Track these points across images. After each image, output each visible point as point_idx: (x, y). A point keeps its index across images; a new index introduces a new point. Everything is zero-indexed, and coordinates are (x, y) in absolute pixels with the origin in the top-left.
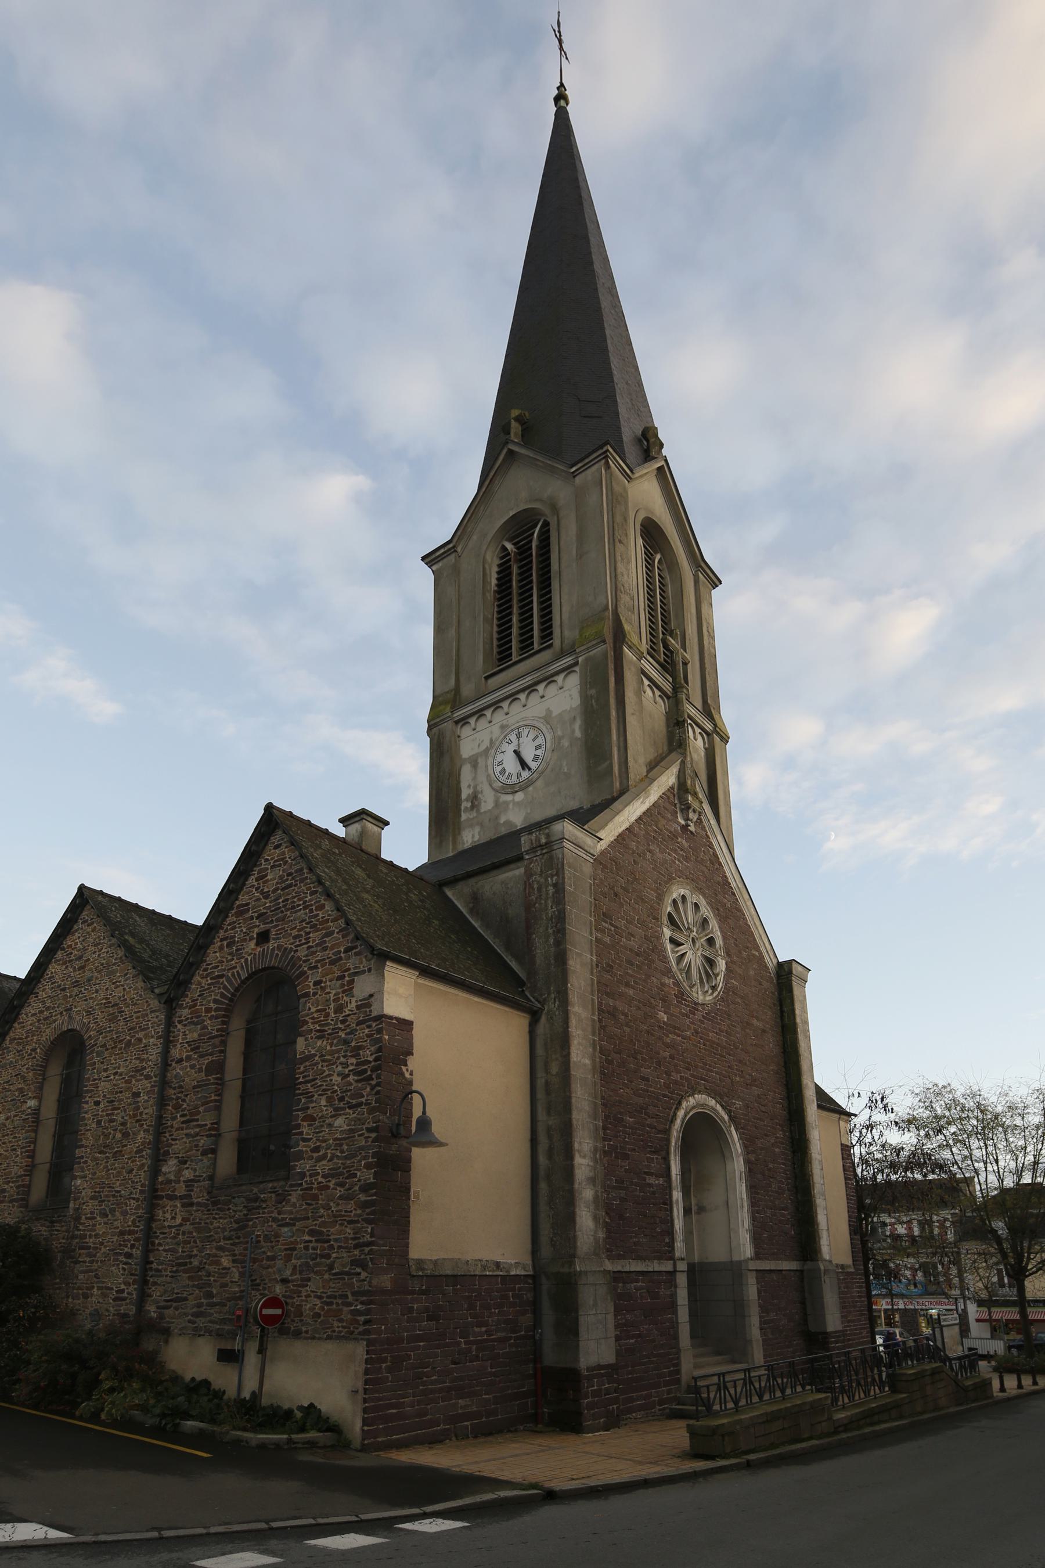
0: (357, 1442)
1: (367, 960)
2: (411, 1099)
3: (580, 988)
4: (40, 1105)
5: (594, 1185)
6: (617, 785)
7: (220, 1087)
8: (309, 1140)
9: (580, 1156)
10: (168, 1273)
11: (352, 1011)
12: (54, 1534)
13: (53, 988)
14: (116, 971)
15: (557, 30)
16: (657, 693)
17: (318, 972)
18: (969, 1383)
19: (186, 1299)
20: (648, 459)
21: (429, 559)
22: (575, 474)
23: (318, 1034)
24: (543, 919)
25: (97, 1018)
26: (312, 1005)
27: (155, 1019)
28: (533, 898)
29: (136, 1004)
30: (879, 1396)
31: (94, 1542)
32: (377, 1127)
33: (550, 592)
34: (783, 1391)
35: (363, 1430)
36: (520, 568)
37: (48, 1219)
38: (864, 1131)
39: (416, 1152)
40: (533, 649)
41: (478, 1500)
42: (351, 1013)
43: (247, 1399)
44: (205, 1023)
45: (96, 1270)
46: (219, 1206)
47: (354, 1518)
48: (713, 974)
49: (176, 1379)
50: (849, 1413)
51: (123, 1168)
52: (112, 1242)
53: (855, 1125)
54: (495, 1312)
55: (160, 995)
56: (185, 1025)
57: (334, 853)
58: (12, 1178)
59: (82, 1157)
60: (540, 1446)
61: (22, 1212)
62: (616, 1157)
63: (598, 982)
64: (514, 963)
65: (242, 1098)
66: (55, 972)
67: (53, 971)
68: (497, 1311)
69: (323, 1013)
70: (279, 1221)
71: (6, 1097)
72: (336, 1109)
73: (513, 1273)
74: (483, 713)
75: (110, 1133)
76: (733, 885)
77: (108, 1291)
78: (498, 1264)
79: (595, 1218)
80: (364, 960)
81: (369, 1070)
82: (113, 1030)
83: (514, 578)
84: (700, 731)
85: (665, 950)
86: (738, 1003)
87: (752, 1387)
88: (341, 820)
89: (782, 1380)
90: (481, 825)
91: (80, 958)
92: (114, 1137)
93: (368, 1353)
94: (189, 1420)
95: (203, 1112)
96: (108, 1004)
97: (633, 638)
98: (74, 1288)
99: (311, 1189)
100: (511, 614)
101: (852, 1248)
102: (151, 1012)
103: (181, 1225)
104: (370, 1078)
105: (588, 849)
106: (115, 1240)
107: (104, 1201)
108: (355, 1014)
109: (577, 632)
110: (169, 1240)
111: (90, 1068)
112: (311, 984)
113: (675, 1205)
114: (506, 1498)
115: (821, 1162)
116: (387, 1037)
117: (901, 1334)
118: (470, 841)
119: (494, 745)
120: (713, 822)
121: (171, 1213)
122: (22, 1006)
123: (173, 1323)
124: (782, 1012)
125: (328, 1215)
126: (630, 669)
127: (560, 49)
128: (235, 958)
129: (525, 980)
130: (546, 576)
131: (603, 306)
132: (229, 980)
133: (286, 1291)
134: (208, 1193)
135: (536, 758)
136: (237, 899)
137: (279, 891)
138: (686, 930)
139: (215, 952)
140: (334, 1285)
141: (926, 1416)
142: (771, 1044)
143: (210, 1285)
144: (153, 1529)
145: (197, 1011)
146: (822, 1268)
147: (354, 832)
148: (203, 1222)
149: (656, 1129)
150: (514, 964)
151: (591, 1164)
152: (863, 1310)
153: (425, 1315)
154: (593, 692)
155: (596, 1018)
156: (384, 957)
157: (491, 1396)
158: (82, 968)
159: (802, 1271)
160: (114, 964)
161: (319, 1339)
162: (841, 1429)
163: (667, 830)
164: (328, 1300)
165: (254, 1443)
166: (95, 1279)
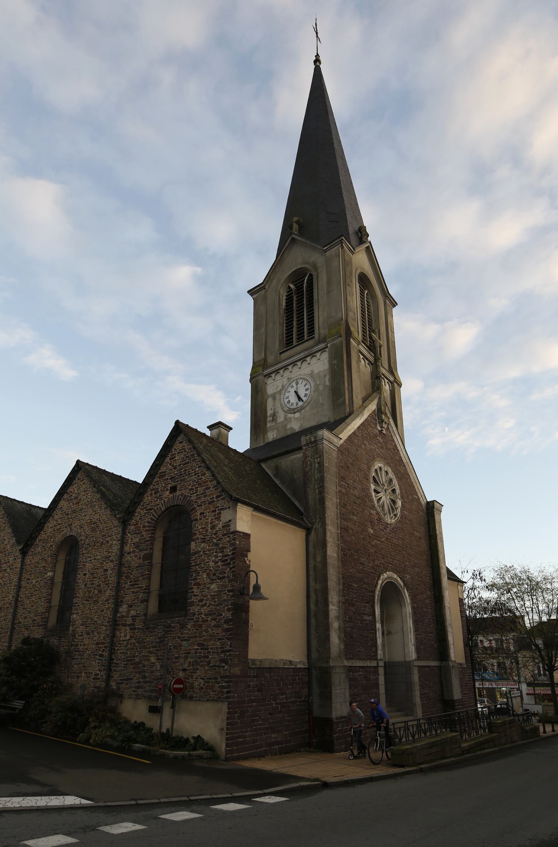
0: (223, 756)
1: (228, 502)
2: (250, 575)
3: (332, 516)
4: (54, 575)
5: (339, 620)
6: (348, 410)
7: (150, 567)
8: (197, 596)
9: (332, 605)
10: (122, 665)
11: (220, 528)
12: (85, 802)
13: (61, 514)
14: (95, 505)
15: (315, 27)
16: (367, 362)
17: (202, 508)
18: (528, 728)
19: (132, 679)
20: (361, 242)
21: (251, 292)
22: (326, 250)
23: (202, 540)
24: (312, 480)
25: (85, 530)
26: (199, 525)
27: (116, 531)
28: (308, 469)
29: (106, 523)
30: (484, 735)
31: (105, 806)
32: (233, 589)
33: (313, 310)
34: (436, 731)
35: (226, 750)
36: (297, 297)
37: (58, 635)
38: (470, 591)
39: (252, 602)
40: (304, 339)
41: (290, 787)
42: (219, 529)
43: (164, 732)
44: (143, 533)
45: (84, 663)
46: (150, 630)
47: (230, 795)
48: (395, 508)
49: (127, 721)
50: (469, 744)
51: (98, 609)
52: (93, 648)
53: (465, 588)
54: (289, 687)
55: (119, 518)
56: (132, 534)
57: (209, 446)
58: (39, 614)
59: (77, 603)
60: (314, 759)
61: (44, 632)
62: (349, 605)
63: (340, 513)
64: (297, 503)
65: (161, 573)
66: (63, 505)
67: (62, 504)
68: (290, 687)
69: (205, 529)
70: (181, 638)
71: (36, 570)
72: (212, 580)
73: (298, 667)
74: (279, 371)
75: (92, 591)
76: (404, 461)
77: (90, 675)
78: (291, 662)
79: (339, 638)
80: (226, 502)
81: (229, 559)
82: (94, 536)
83: (294, 303)
84: (387, 381)
85: (372, 496)
86: (408, 524)
87: (409, 732)
88: (208, 427)
89: (436, 726)
90: (278, 430)
91: (76, 498)
92: (94, 592)
93: (229, 708)
94: (136, 744)
95: (141, 580)
96: (91, 522)
97: (355, 334)
98: (72, 673)
99: (198, 621)
100: (293, 320)
101: (465, 654)
102: (114, 527)
103: (129, 640)
104: (229, 564)
105: (335, 444)
106: (94, 647)
107: (88, 626)
108: (222, 530)
109: (327, 331)
110: (123, 648)
111: (81, 556)
112: (199, 514)
113: (377, 631)
114: (304, 786)
115: (449, 608)
116: (238, 542)
117: (488, 702)
118: (272, 438)
119: (284, 388)
120: (394, 428)
121: (124, 633)
122: (45, 523)
123: (125, 691)
124: (429, 528)
125: (207, 635)
126: (354, 350)
127: (317, 37)
128: (158, 500)
129: (303, 512)
130: (311, 302)
131: (339, 166)
132: (155, 511)
133: (185, 675)
134: (144, 623)
135: (306, 395)
136: (160, 469)
137: (182, 466)
138: (382, 485)
139: (148, 496)
140: (210, 673)
141: (508, 746)
142: (424, 545)
143: (144, 672)
144: (132, 800)
145: (138, 527)
146: (451, 665)
147: (215, 433)
148: (141, 638)
149: (368, 590)
150: (297, 503)
151: (337, 609)
152: (471, 688)
153: (256, 688)
154: (335, 362)
155: (339, 532)
156: (236, 501)
157: (288, 732)
158: (78, 503)
159: (441, 667)
160: (94, 502)
161: (202, 701)
162: (465, 752)
163: (372, 433)
164: (207, 680)
165: (171, 756)
166: (83, 668)
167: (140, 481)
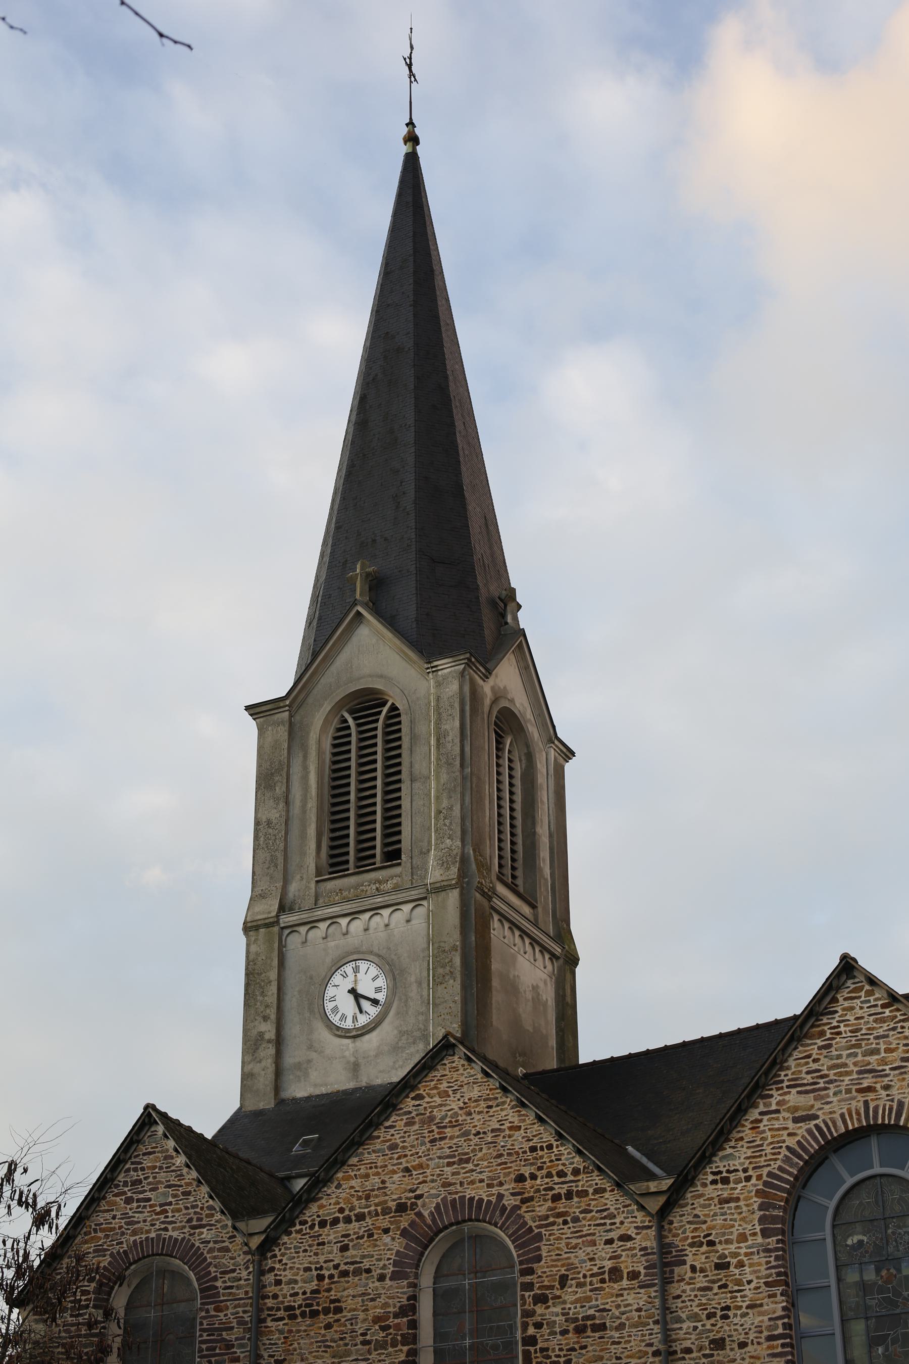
167: (209, 1136)
